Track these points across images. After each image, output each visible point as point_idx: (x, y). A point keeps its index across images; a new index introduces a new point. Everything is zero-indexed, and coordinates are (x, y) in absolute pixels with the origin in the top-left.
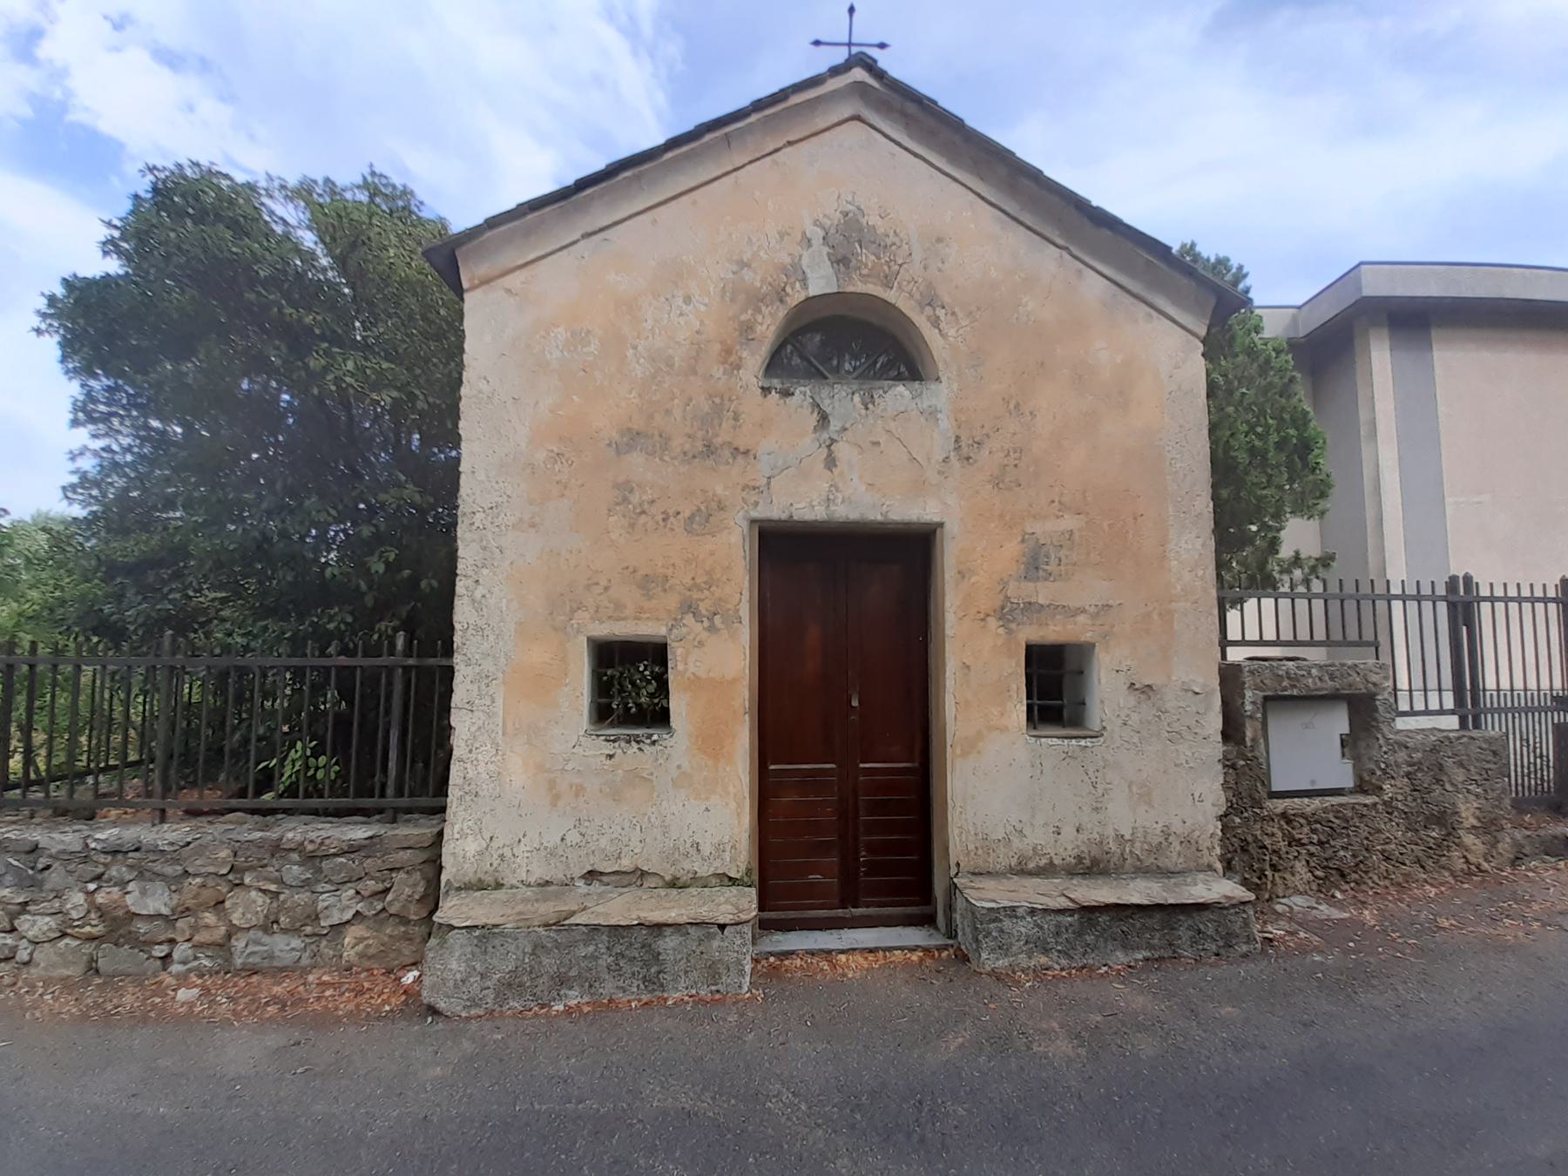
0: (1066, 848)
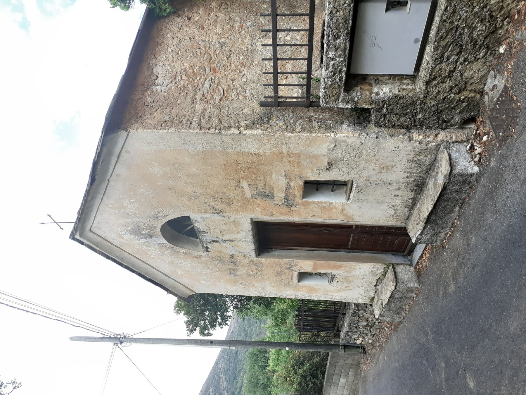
0: (407, 195)
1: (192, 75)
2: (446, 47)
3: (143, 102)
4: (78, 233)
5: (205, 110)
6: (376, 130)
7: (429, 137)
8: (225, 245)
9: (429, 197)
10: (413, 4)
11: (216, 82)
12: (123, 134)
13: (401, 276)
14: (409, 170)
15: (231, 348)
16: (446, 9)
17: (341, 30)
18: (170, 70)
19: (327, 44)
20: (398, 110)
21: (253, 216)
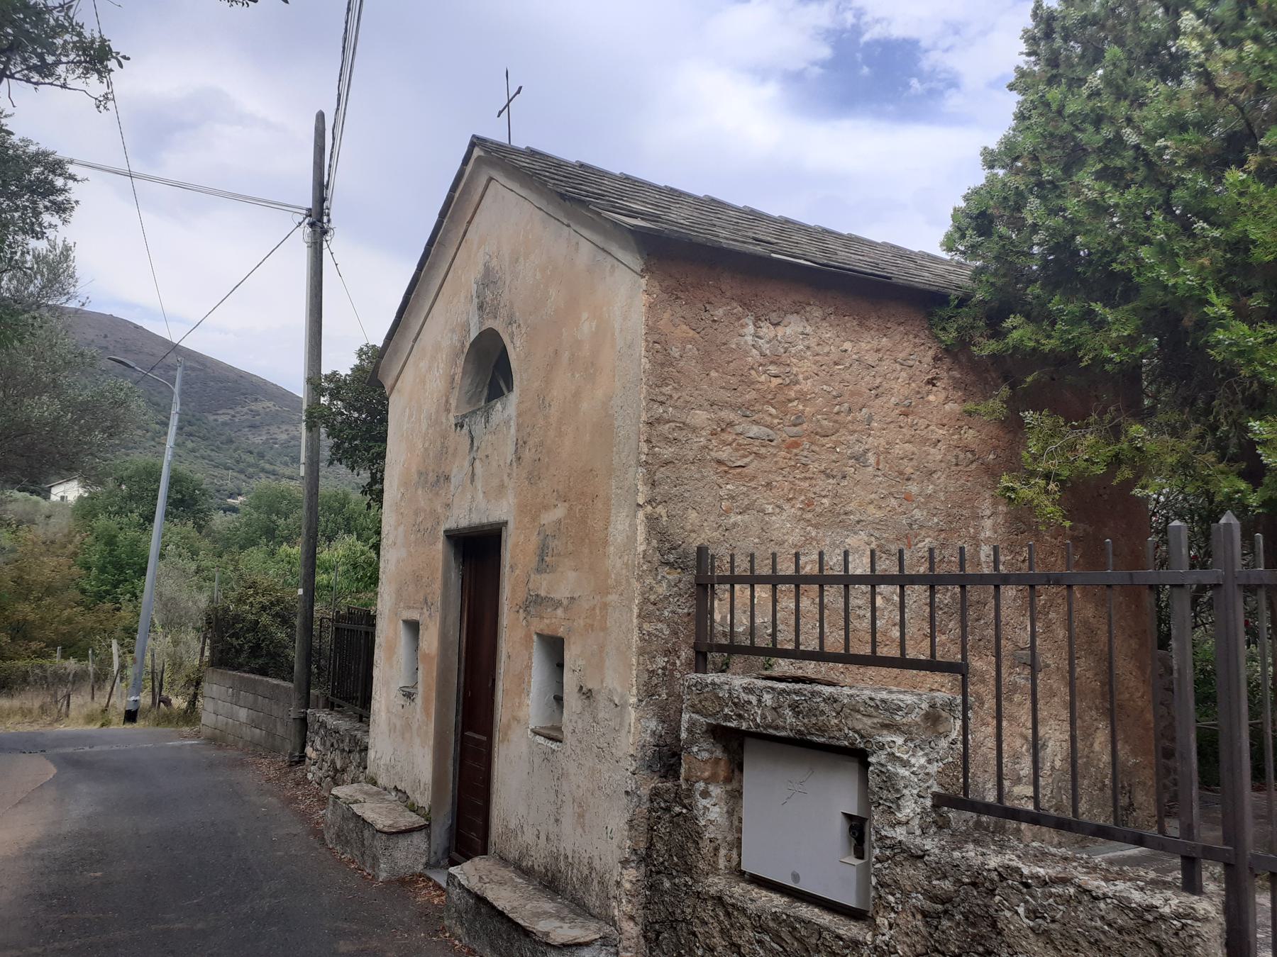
0: (538, 859)
1: (780, 397)
2: (777, 938)
3: (713, 299)
4: (482, 154)
5: (694, 430)
6: (645, 791)
7: (630, 902)
8: (466, 464)
9: (522, 902)
10: (854, 869)
11: (763, 451)
12: (636, 262)
13: (403, 842)
14: (577, 861)
15: (302, 468)
16: (839, 937)
17: (806, 721)
18: (793, 350)
19: (784, 690)
20: (677, 837)
21: (511, 526)
